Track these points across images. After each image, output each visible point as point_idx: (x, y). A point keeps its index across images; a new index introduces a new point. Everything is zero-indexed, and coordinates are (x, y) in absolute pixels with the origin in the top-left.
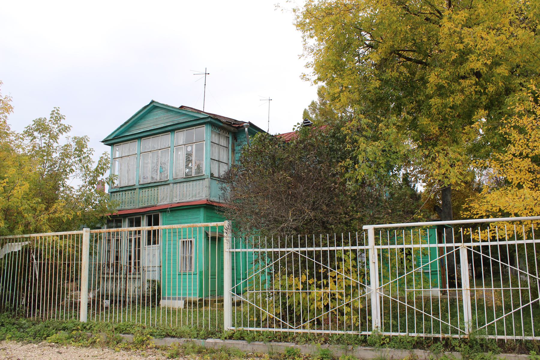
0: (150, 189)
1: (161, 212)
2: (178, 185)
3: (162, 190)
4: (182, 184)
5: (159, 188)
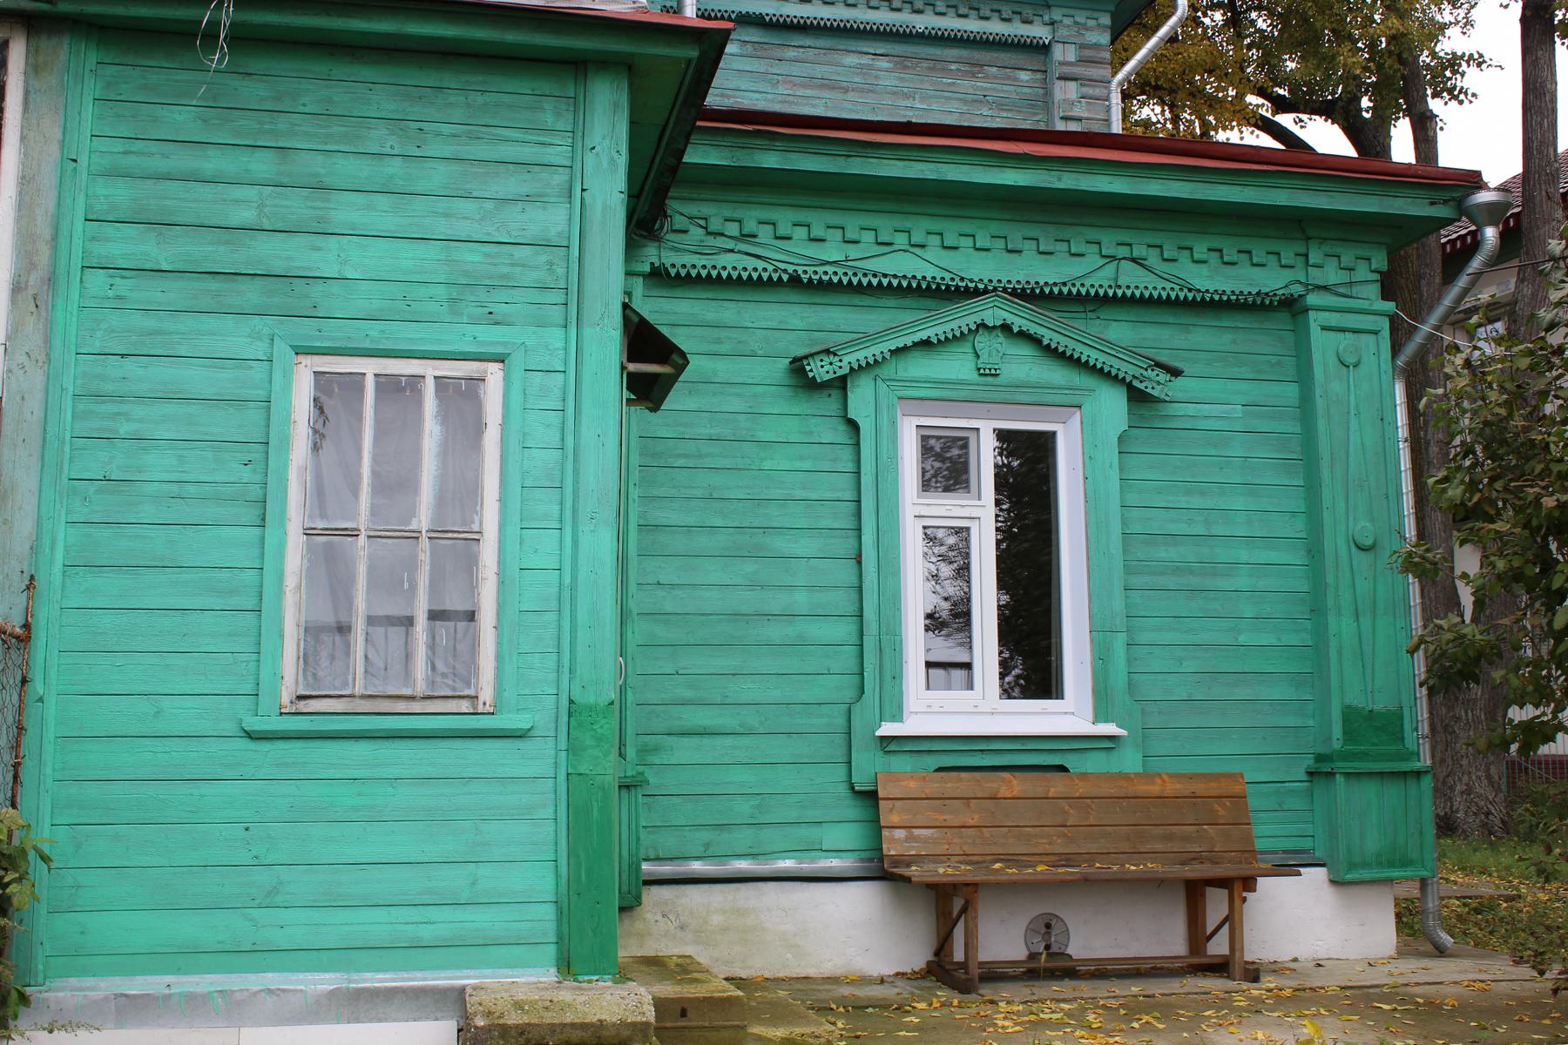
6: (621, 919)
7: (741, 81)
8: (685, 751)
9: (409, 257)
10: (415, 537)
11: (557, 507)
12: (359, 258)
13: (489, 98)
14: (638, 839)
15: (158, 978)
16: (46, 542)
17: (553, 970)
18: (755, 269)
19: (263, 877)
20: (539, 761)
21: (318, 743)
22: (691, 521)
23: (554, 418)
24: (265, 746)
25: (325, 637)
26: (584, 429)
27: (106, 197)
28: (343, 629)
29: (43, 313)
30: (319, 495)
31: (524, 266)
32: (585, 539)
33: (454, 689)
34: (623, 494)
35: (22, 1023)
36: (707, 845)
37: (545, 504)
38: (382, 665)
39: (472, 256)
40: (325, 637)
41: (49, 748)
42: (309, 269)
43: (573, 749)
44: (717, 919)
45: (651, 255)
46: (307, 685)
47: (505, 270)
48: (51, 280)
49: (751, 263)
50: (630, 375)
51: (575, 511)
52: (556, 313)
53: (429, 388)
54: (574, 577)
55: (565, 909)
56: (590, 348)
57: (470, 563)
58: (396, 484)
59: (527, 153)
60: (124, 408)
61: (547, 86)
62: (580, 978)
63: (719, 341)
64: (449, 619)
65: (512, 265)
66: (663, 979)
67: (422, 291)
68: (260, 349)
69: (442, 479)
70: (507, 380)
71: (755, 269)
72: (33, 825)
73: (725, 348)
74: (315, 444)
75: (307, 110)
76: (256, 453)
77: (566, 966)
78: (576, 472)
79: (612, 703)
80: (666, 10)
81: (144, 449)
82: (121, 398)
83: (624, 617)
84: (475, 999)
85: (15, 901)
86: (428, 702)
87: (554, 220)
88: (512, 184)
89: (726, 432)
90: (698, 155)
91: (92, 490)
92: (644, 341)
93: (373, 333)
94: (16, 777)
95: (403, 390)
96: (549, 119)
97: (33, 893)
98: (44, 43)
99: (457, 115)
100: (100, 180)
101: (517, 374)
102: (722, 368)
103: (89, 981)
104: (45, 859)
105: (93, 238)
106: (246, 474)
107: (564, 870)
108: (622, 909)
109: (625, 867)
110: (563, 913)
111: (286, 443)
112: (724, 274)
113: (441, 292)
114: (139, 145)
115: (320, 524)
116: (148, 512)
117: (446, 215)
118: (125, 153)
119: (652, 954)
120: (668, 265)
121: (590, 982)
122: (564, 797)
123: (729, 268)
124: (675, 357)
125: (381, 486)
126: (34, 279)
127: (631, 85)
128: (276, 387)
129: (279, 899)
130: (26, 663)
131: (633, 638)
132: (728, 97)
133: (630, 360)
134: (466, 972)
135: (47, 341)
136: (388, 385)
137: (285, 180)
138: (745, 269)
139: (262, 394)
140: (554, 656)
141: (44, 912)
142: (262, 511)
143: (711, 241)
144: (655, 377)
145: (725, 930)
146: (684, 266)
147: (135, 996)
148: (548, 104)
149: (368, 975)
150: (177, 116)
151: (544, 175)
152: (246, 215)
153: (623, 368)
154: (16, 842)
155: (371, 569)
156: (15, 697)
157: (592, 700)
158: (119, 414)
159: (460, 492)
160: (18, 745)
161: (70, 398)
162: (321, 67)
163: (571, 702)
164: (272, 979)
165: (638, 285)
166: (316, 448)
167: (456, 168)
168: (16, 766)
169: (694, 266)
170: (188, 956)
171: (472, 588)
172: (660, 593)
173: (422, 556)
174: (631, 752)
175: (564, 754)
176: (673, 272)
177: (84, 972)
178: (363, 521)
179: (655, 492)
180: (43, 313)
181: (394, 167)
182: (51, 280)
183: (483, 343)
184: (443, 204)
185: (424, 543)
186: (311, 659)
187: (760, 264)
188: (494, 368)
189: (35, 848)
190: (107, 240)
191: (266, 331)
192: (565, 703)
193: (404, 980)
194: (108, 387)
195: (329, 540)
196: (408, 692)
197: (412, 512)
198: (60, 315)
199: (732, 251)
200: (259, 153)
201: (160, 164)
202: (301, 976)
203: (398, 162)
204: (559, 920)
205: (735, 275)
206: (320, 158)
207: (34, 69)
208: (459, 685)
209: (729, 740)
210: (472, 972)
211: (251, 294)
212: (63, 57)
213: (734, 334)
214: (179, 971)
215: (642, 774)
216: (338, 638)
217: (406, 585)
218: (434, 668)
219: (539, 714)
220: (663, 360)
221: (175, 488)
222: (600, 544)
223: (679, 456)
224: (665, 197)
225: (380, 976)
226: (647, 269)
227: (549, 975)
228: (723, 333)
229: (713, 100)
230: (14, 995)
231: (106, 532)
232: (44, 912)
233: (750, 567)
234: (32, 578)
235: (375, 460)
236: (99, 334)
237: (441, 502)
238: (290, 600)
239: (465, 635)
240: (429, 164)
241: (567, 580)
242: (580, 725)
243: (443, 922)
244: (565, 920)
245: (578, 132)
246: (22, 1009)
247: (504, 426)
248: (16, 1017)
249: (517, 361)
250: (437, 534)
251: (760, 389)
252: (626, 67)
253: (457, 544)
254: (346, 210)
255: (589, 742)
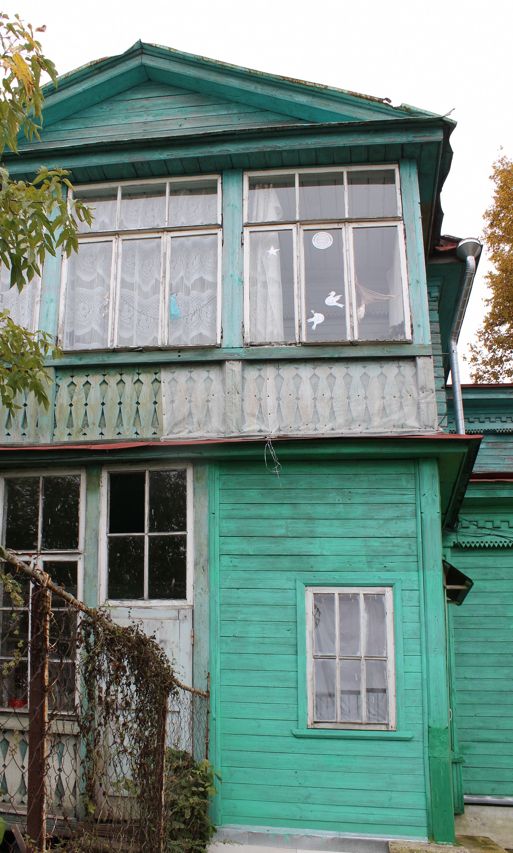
0: (113, 379)
1: (195, 462)
2: (270, 371)
3: (175, 385)
4: (288, 372)
5: (164, 376)
6: (455, 819)
7: (487, 460)
8: (480, 749)
9: (349, 545)
10: (359, 659)
11: (419, 647)
12: (328, 547)
13: (377, 477)
14: (461, 785)
15: (264, 827)
16: (213, 661)
17: (426, 838)
18: (501, 542)
19: (303, 791)
20: (417, 751)
21: (323, 741)
22: (479, 651)
23: (416, 610)
24: (302, 741)
25: (324, 698)
26: (429, 614)
27: (227, 527)
28: (331, 695)
29: (207, 573)
30: (318, 642)
31: (398, 546)
32: (432, 659)
33: (378, 721)
34: (447, 641)
35: (214, 839)
36: (493, 790)
37: (414, 645)
38: (348, 710)
39: (376, 543)
40: (324, 698)
41: (219, 737)
42: (309, 552)
43: (431, 747)
44: (499, 822)
45: (453, 539)
46: (318, 718)
47: (391, 548)
48: (208, 560)
49: (499, 539)
50: (448, 590)
51: (427, 648)
52: (414, 565)
53: (362, 598)
54: (428, 676)
55: (430, 813)
56: (429, 579)
57: (383, 669)
58: (350, 637)
59: (395, 499)
60: (239, 609)
61: (402, 470)
62: (439, 842)
63: (486, 574)
64: (375, 692)
65: (393, 546)
66: (476, 846)
67: (356, 559)
68: (291, 585)
69: (369, 635)
70: (394, 594)
71: (501, 542)
72: (214, 766)
73: (489, 577)
74: (316, 623)
75: (303, 487)
76: (292, 626)
77: (432, 837)
78: (426, 632)
79: (447, 728)
80: (451, 432)
81: (248, 625)
82: (238, 605)
83: (451, 692)
84: (393, 847)
85: (210, 793)
86: (368, 726)
87: (410, 526)
88: (390, 512)
89: (493, 613)
90: (471, 494)
91: (229, 641)
92: (452, 575)
93: (336, 577)
94: (207, 748)
95: (350, 599)
96: (404, 484)
97: (216, 791)
98: (200, 469)
99: (365, 485)
100: (224, 520)
101: (399, 592)
102: (489, 586)
103: (238, 826)
104: (220, 779)
105: (223, 543)
106: (289, 634)
107: (429, 796)
108: (456, 814)
109: (456, 797)
110: (430, 815)
111: (304, 622)
112: (487, 545)
113: (363, 559)
114: (238, 506)
115: (320, 654)
116: (251, 649)
117: (364, 527)
118: (232, 509)
119: (470, 835)
120: (461, 543)
121: (443, 844)
122: (428, 766)
123: (489, 542)
124: (467, 582)
125: (343, 637)
126: (202, 560)
127: (439, 467)
128: (298, 599)
129: (310, 801)
130: (208, 706)
131: (455, 700)
132: (483, 467)
133: (448, 584)
134: (388, 836)
135: (209, 583)
136: (343, 597)
137: (296, 516)
138: (496, 542)
139: (293, 602)
140: (421, 708)
141: (220, 798)
142: (296, 649)
143: (480, 531)
144: (459, 591)
145: (504, 827)
146: (468, 542)
147: (255, 833)
148: (403, 477)
149: (348, 833)
150: (251, 494)
151: (404, 507)
152: (281, 531)
153: (444, 588)
154: (208, 772)
155: (342, 672)
156: (205, 718)
157: (438, 726)
158: (237, 611)
159: (377, 640)
160: (207, 736)
161: (218, 605)
162: (306, 469)
163: (429, 727)
164: (308, 831)
165: (449, 552)
166: (316, 625)
167: (365, 507)
168: (207, 744)
169: (473, 542)
170: (274, 820)
171: (384, 678)
172: (466, 682)
173: (362, 667)
174: (456, 749)
175: (427, 748)
176: (464, 545)
177: (236, 822)
178: (337, 652)
179: (462, 639)
180: (207, 573)
181: (340, 509)
182: (208, 560)
183: (383, 579)
184: (361, 522)
185: (363, 661)
186: (319, 707)
187: (503, 540)
188: (388, 589)
189: (216, 774)
190: (228, 544)
191: (293, 577)
192: (427, 727)
193: (362, 836)
194: (233, 601)
195: (324, 661)
196: (359, 721)
197: (357, 649)
198: (212, 573)
199: (490, 535)
200: (285, 506)
201: (247, 513)
202: (320, 831)
203: (341, 506)
204: (428, 817)
205: (492, 545)
206: (309, 507)
207: (196, 479)
208: (380, 719)
209: (501, 745)
210: (391, 836)
211: (286, 563)
212: (207, 473)
213: (493, 571)
214: (272, 825)
215: (462, 758)
216: (329, 699)
217: (356, 679)
218: (369, 712)
219: (415, 731)
220: (462, 583)
221: (261, 640)
222: (439, 662)
223: (471, 624)
224: (458, 513)
225: (353, 834)
226: (452, 544)
227: (425, 840)
228: (488, 571)
229: (476, 469)
230: (211, 828)
231: (235, 657)
232: (220, 798)
233: (506, 671)
234: (209, 674)
235: (341, 628)
236: (228, 580)
237: (369, 644)
238: (309, 684)
239: (382, 699)
240: (355, 506)
241: (425, 677)
242: (434, 737)
243: (378, 815)
244: (430, 817)
245: (417, 489)
246: (214, 833)
247: (394, 613)
248: (212, 837)
249: (398, 586)
250: (368, 658)
251: (506, 594)
252: (436, 459)
253: (377, 662)
254: (322, 528)
255: (438, 744)
